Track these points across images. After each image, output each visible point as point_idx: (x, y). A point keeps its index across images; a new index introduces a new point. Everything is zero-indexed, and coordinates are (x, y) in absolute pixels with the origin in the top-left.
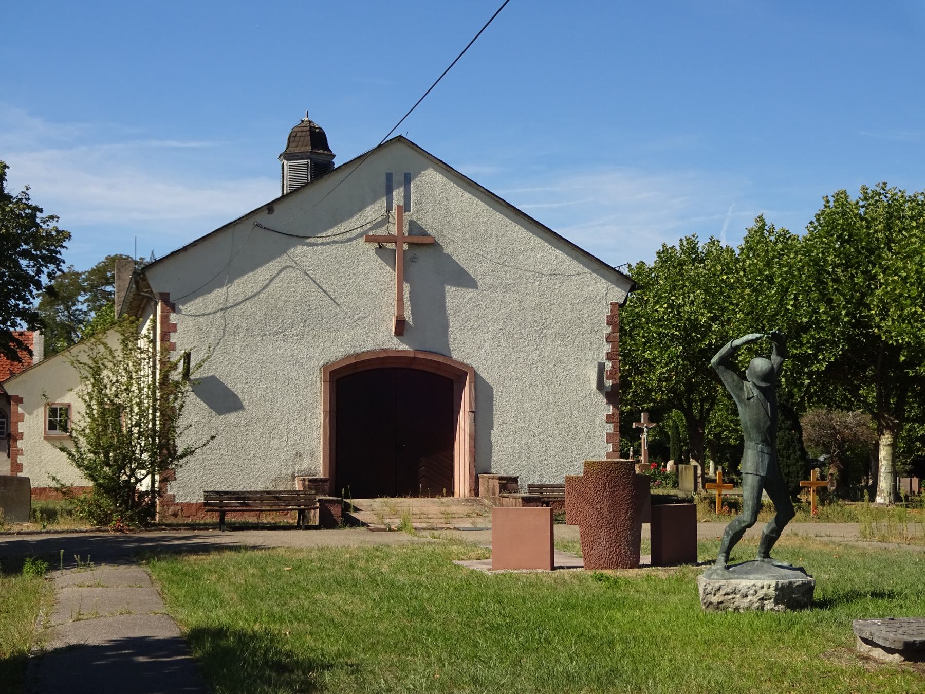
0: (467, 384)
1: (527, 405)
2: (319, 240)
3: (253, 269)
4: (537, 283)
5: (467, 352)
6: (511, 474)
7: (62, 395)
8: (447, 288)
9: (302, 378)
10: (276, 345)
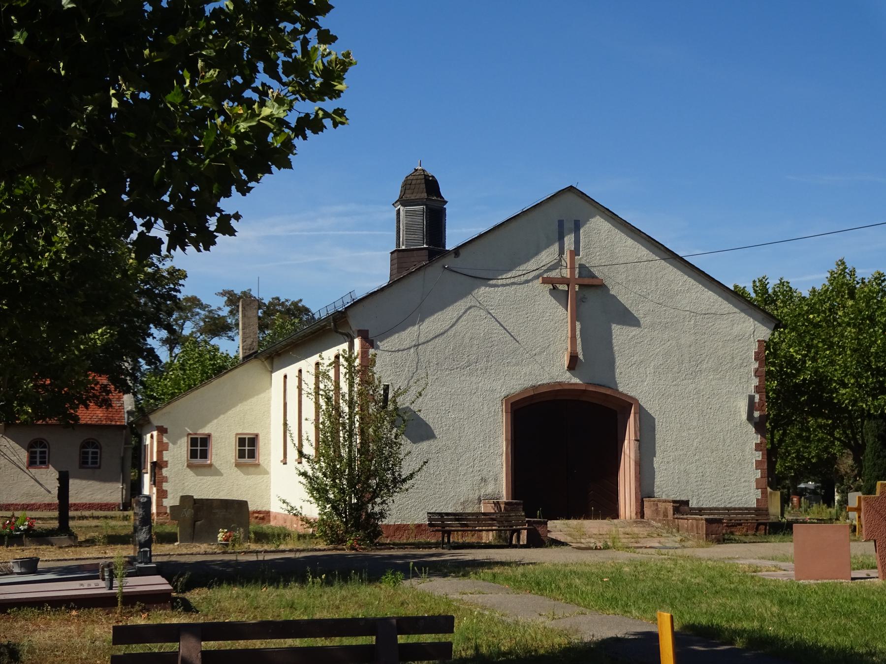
0: (632, 416)
1: (684, 434)
2: (500, 282)
3: (442, 309)
4: (692, 322)
5: (630, 386)
6: (684, 498)
7: (204, 425)
8: (614, 326)
9: (485, 409)
10: (463, 378)
